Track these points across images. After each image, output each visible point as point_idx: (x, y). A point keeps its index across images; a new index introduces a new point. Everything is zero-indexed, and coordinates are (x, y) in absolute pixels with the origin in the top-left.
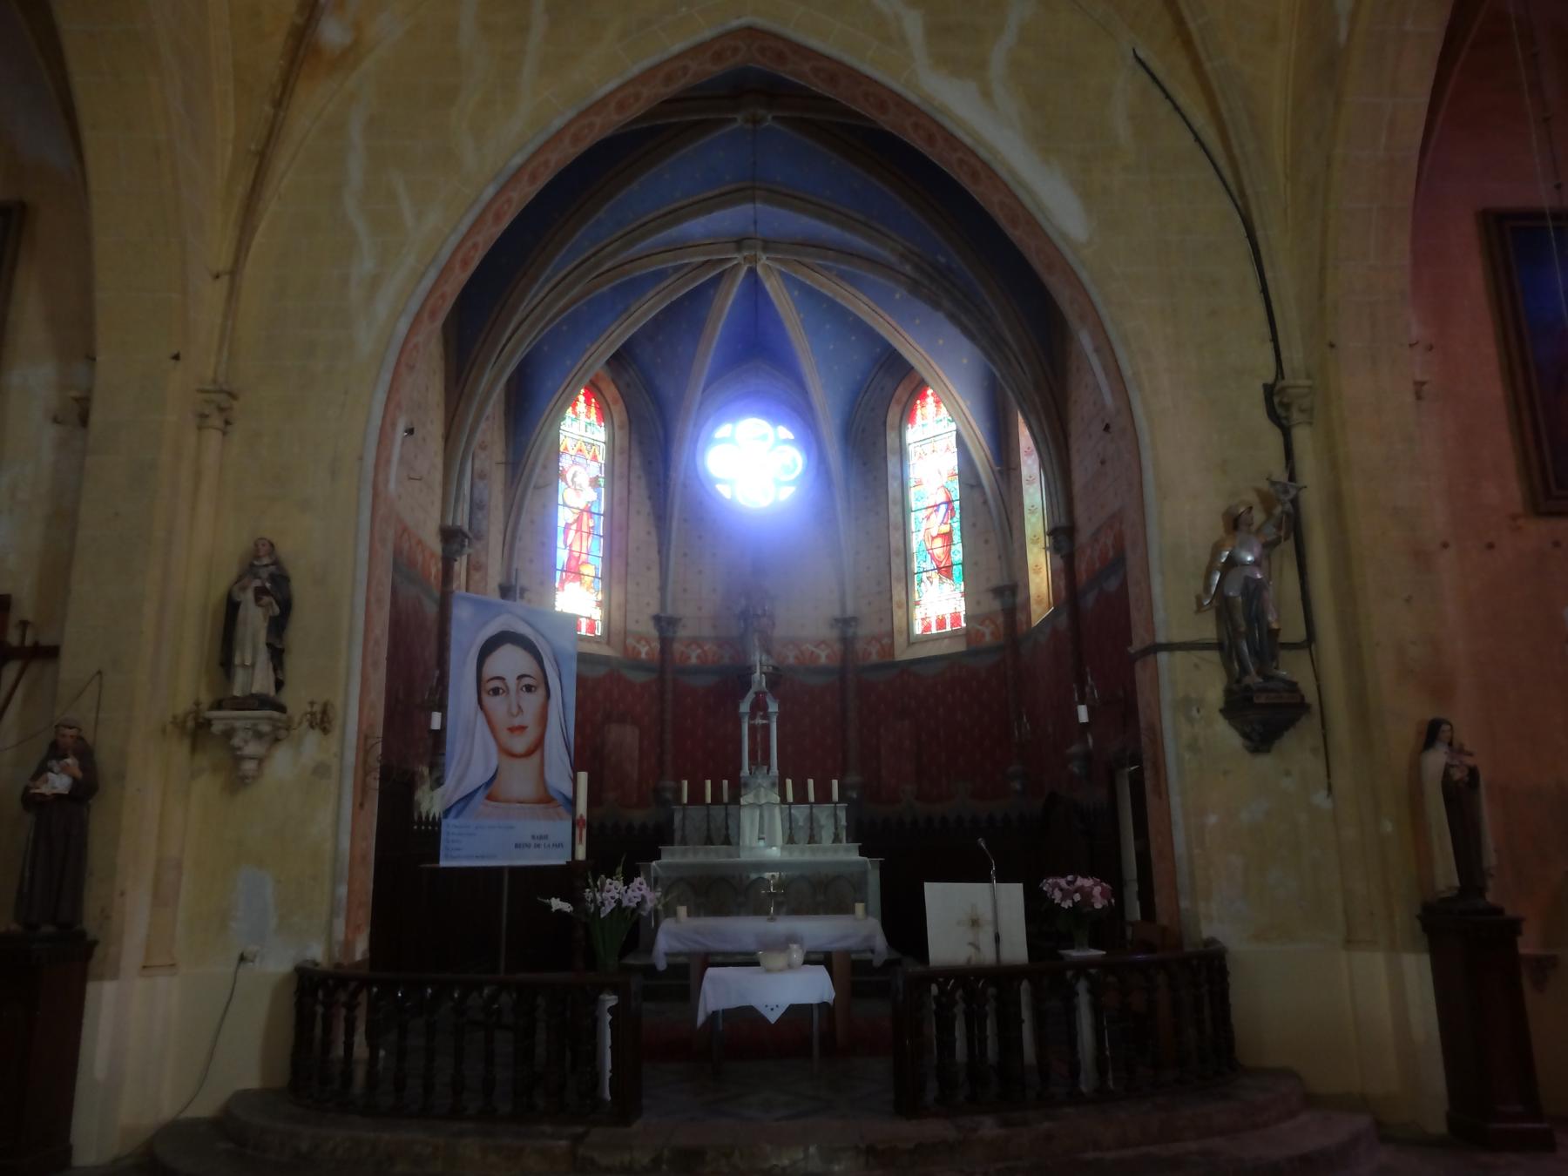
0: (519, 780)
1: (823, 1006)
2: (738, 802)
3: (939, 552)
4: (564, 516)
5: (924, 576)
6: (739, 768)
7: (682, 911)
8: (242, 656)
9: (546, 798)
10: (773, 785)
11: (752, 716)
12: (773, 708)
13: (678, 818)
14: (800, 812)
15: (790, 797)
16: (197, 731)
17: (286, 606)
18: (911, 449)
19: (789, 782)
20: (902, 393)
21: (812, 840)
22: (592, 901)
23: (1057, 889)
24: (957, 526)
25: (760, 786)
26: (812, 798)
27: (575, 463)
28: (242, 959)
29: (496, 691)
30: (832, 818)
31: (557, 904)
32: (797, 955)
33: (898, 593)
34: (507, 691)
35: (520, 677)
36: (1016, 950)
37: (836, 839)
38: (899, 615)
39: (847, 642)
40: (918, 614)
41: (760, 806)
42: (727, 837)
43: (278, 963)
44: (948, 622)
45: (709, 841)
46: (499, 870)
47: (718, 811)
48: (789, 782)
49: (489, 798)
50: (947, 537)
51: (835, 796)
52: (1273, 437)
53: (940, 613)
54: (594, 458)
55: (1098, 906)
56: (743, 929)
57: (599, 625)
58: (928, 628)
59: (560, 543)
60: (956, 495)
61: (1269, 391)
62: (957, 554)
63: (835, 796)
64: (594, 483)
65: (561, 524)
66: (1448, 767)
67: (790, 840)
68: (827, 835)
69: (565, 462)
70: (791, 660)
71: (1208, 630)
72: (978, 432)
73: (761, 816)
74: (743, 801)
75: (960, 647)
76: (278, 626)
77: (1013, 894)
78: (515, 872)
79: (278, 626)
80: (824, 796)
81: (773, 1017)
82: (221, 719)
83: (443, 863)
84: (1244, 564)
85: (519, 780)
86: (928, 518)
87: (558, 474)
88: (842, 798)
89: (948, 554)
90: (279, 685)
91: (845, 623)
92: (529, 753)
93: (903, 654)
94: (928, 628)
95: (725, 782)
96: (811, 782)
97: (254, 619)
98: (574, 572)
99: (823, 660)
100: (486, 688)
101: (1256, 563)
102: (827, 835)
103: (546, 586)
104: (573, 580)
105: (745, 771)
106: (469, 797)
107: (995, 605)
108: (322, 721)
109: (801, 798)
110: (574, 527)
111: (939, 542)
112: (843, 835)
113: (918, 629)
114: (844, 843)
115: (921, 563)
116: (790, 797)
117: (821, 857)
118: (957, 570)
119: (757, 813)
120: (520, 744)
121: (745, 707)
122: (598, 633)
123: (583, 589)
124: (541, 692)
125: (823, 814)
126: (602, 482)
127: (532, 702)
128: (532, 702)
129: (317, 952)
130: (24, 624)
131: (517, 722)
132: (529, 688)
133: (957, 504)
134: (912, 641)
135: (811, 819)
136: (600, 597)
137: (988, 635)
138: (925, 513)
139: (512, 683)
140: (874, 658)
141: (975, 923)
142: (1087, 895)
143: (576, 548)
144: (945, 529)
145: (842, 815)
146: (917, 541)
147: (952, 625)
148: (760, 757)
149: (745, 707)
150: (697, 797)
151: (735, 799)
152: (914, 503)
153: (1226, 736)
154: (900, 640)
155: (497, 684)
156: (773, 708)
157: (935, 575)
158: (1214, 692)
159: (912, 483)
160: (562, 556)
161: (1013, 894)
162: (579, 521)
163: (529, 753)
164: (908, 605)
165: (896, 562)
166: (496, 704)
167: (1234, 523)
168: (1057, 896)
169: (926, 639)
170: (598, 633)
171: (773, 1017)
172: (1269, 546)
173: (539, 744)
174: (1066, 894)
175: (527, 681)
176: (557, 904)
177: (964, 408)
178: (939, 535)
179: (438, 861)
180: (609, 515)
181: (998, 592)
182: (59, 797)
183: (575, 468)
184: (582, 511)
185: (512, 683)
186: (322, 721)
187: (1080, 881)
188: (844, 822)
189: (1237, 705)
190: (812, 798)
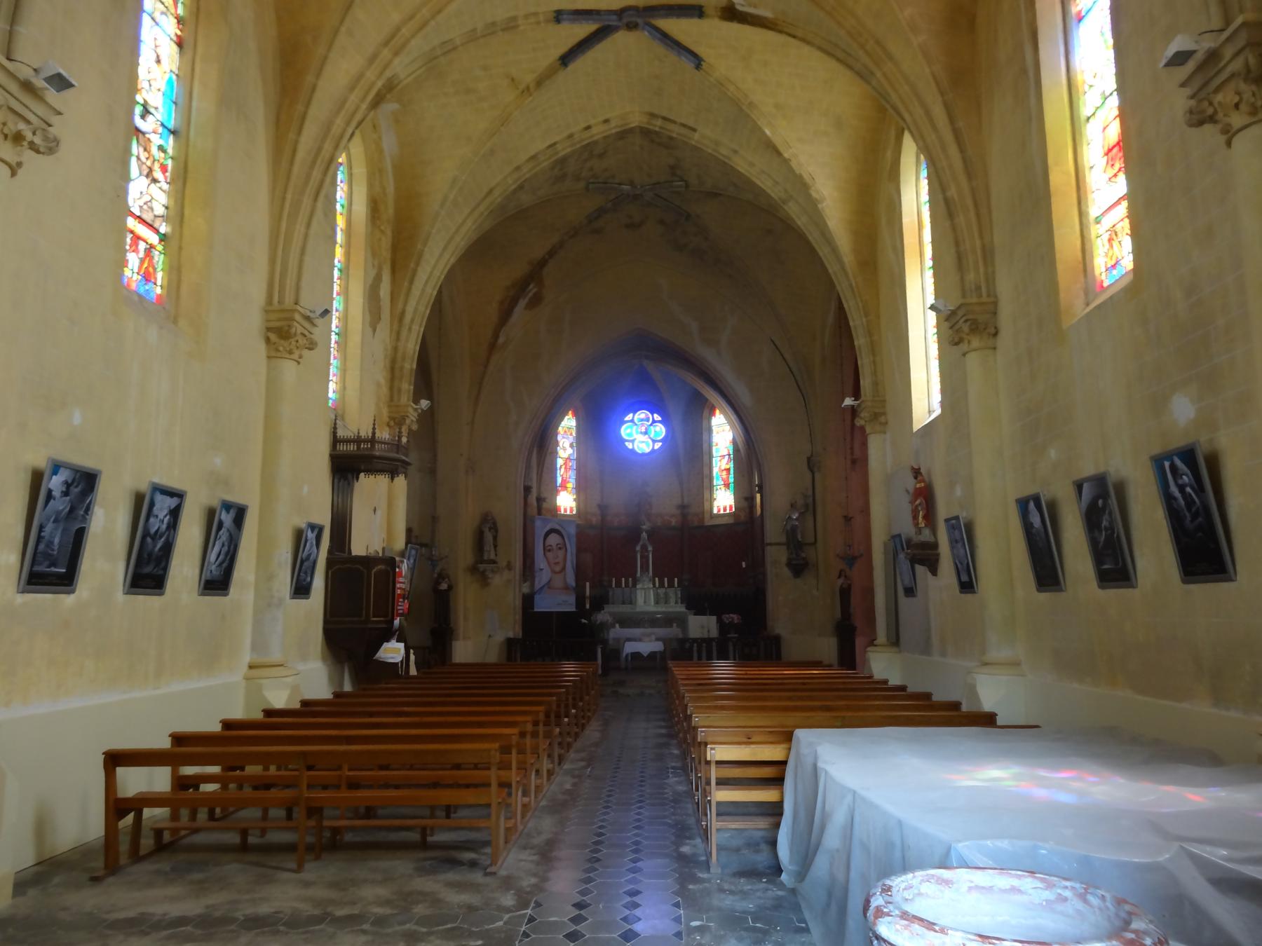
0: (558, 581)
1: (660, 652)
2: (636, 587)
3: (725, 477)
4: (560, 462)
5: (718, 487)
6: (636, 571)
7: (617, 625)
8: (486, 548)
9: (567, 588)
10: (650, 580)
11: (642, 552)
12: (650, 548)
13: (611, 593)
14: (661, 591)
15: (657, 585)
16: (473, 569)
17: (497, 531)
18: (713, 428)
19: (657, 579)
20: (706, 413)
21: (666, 603)
22: (1106, 529)
23: (727, 618)
24: (732, 466)
25: (644, 581)
26: (666, 585)
27: (563, 438)
28: (490, 636)
29: (549, 551)
30: (674, 594)
31: (583, 621)
32: (653, 637)
33: (706, 495)
34: (553, 549)
35: (557, 544)
36: (714, 633)
37: (676, 603)
38: (706, 505)
39: (684, 516)
40: (716, 504)
41: (644, 589)
42: (631, 602)
43: (500, 637)
44: (728, 509)
45: (624, 603)
46: (551, 613)
47: (627, 590)
48: (657, 579)
49: (549, 588)
50: (728, 470)
51: (676, 585)
52: (809, 475)
53: (725, 504)
54: (571, 434)
55: (736, 622)
56: (637, 632)
57: (575, 509)
58: (719, 510)
59: (558, 475)
60: (731, 452)
61: (809, 459)
62: (731, 480)
63: (676, 585)
64: (571, 446)
65: (558, 466)
66: (843, 584)
67: (657, 602)
68: (672, 600)
69: (559, 438)
70: (659, 524)
71: (783, 539)
72: (739, 429)
73: (645, 593)
74: (638, 587)
75: (731, 521)
76: (495, 538)
77: (714, 618)
78: (558, 613)
79: (495, 538)
80: (671, 585)
81: (645, 655)
82: (482, 567)
83: (536, 610)
84: (793, 519)
85: (558, 581)
86: (720, 461)
87: (557, 444)
88: (678, 586)
89: (728, 478)
90: (496, 555)
91: (683, 507)
92: (560, 572)
93: (708, 522)
94: (719, 510)
95: (630, 579)
96: (666, 579)
97: (489, 536)
98: (564, 487)
99: (673, 524)
100: (546, 549)
101: (797, 519)
102: (672, 600)
103: (555, 492)
104: (564, 491)
105: (639, 574)
106: (544, 586)
107: (745, 504)
108: (509, 567)
109: (662, 585)
110: (563, 467)
111: (725, 473)
112: (679, 601)
113: (715, 511)
114: (680, 604)
115: (718, 481)
116: (657, 585)
117: (671, 610)
118: (732, 486)
119: (643, 592)
120: (558, 569)
121: (638, 548)
122: (574, 513)
123: (568, 494)
124: (563, 551)
125: (671, 592)
126: (575, 445)
127: (561, 553)
128: (561, 553)
129: (511, 635)
130: (417, 537)
131: (557, 561)
132: (560, 548)
133: (732, 456)
134: (712, 516)
135: (666, 594)
136: (575, 497)
137: (743, 517)
138: (719, 458)
139: (554, 547)
140: (696, 524)
141: (703, 627)
142: (733, 618)
143: (565, 476)
144: (728, 467)
145: (679, 593)
146: (715, 471)
147: (730, 510)
148: (645, 568)
149: (638, 548)
150: (618, 584)
151: (634, 585)
152: (715, 454)
153: (787, 572)
154: (707, 516)
155: (550, 547)
156: (650, 548)
157: (723, 488)
158: (784, 559)
159: (714, 444)
160: (559, 480)
161: (714, 618)
162: (565, 464)
163: (560, 572)
164: (712, 500)
165: (706, 481)
166: (549, 554)
167: (793, 506)
168: (725, 619)
169: (719, 516)
170: (574, 513)
171: (645, 655)
172: (801, 514)
173: (564, 569)
174: (727, 619)
175: (559, 546)
176: (583, 621)
177: (733, 418)
178: (725, 469)
179: (533, 609)
180: (578, 460)
181: (746, 499)
182: (445, 590)
183: (564, 440)
184: (567, 459)
185: (554, 547)
186: (509, 567)
187: (731, 615)
188: (679, 596)
189: (790, 564)
190: (666, 585)
